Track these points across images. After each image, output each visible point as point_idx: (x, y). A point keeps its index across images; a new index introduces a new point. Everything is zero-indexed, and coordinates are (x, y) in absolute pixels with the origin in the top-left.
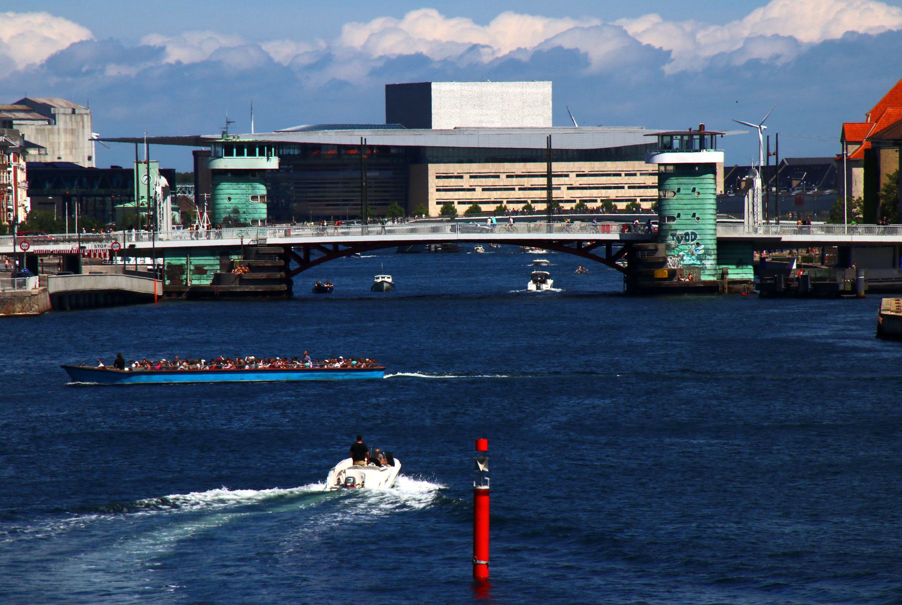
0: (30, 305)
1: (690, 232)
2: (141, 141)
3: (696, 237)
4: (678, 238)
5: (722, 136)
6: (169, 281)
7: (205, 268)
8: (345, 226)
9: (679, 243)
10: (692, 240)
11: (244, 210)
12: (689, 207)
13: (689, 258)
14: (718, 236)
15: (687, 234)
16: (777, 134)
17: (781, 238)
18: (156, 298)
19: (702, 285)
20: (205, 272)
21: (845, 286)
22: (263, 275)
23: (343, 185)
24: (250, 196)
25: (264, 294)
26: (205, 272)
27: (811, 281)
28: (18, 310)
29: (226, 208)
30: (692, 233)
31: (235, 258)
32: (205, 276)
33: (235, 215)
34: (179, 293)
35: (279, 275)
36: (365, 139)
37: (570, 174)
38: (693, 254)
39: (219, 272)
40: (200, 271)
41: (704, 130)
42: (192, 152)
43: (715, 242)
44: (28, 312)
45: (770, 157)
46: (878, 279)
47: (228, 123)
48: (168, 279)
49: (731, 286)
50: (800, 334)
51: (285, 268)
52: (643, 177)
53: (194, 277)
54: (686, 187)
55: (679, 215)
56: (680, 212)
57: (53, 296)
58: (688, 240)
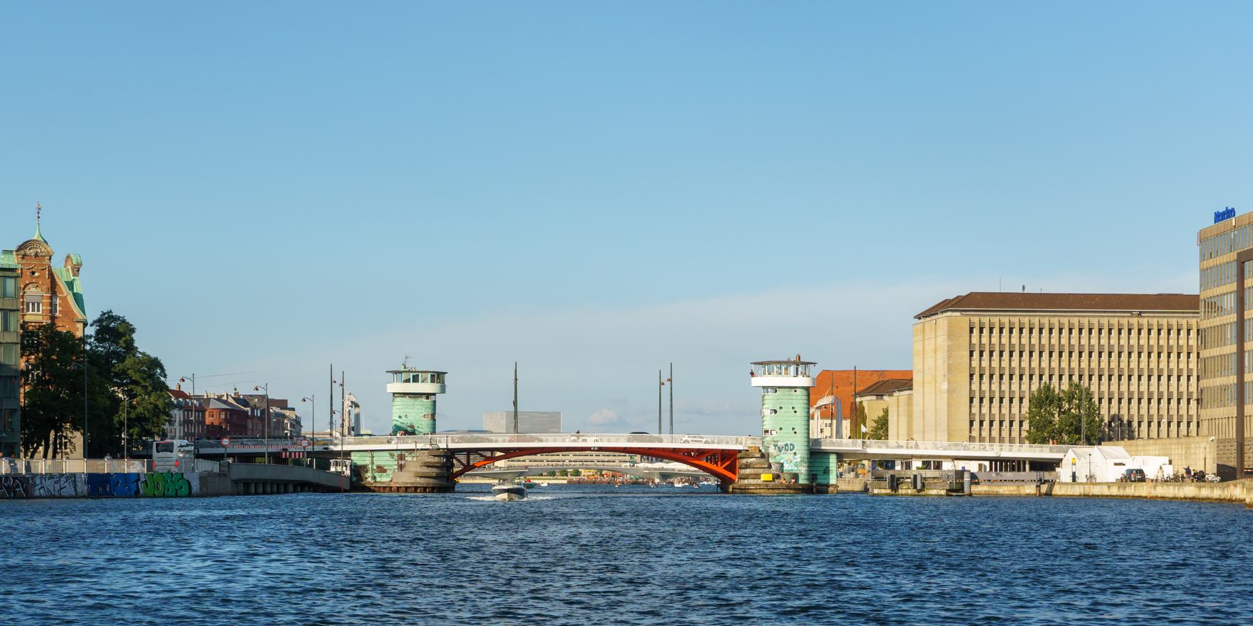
1: (789, 443)
2: (1241, 372)
3: (793, 448)
4: (779, 448)
7: (385, 468)
8: (558, 491)
9: (780, 452)
10: (791, 450)
13: (788, 465)
15: (786, 445)
20: (385, 471)
23: (1188, 562)
26: (385, 471)
30: (791, 444)
36: (1215, 303)
38: (791, 461)
40: (381, 469)
42: (1195, 239)
47: (406, 358)
50: (649, 465)
56: (347, 403)
57: (236, 482)
58: (788, 450)
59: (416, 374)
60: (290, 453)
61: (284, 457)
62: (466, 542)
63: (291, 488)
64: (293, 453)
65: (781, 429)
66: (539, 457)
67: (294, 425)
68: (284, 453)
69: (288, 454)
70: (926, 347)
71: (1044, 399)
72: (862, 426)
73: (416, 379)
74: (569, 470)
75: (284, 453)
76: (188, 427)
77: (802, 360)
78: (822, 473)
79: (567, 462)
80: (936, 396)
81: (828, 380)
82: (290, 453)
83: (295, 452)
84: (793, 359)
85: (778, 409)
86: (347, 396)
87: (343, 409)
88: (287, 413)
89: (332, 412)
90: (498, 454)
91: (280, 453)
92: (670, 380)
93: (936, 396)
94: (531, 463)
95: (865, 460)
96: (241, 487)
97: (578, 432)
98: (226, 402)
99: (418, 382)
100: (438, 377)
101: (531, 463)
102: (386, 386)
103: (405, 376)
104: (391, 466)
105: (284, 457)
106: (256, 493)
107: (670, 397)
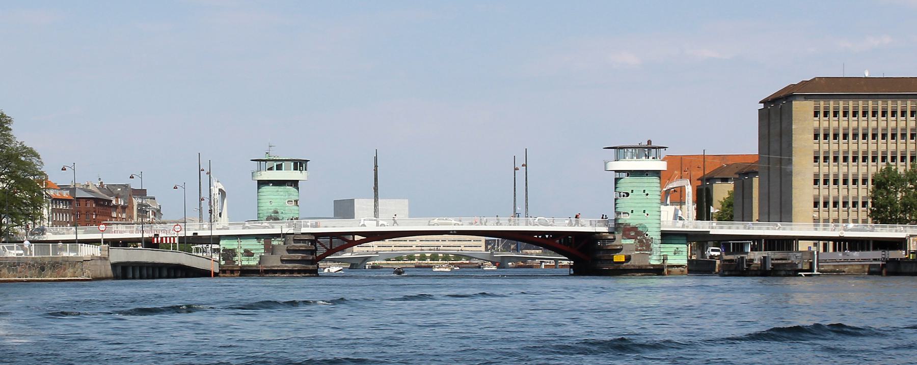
0: (82, 269)
5: (665, 150)
6: (224, 262)
7: (252, 252)
11: (282, 211)
12: (640, 205)
14: (662, 229)
16: (704, 150)
17: (709, 232)
18: (212, 274)
19: (652, 268)
20: (252, 255)
21: (802, 265)
22: (299, 256)
24: (287, 200)
25: (299, 271)
26: (252, 255)
27: (746, 262)
28: (69, 274)
29: (268, 209)
31: (275, 242)
32: (252, 257)
33: (275, 215)
34: (232, 272)
35: (311, 257)
37: (417, 240)
39: (263, 254)
40: (248, 253)
41: (651, 144)
43: (660, 233)
44: (80, 277)
45: (655, 180)
46: (870, 259)
48: (223, 260)
49: (670, 269)
51: (313, 252)
52: (449, 242)
53: (243, 258)
54: (638, 189)
55: (632, 212)
57: (114, 266)
59: (279, 163)
60: (162, 238)
61: (156, 242)
62: (85, 306)
63: (165, 273)
64: (164, 239)
65: (395, 215)
66: (387, 242)
67: (155, 213)
68: (156, 239)
69: (159, 239)
70: (772, 131)
71: (881, 183)
72: (711, 207)
73: (279, 168)
74: (416, 255)
75: (156, 239)
76: (56, 215)
77: (653, 144)
78: (673, 254)
79: (414, 248)
80: (781, 179)
81: (679, 164)
82: (162, 238)
83: (166, 238)
84: (645, 143)
85: (630, 192)
86: (214, 183)
87: (210, 196)
88: (148, 202)
89: (201, 199)
90: (357, 238)
91: (151, 239)
92: (516, 169)
93: (781, 179)
94: (379, 249)
95: (710, 241)
96: (119, 270)
97: (497, 216)
98: (90, 192)
99: (282, 170)
100: (299, 164)
101: (379, 249)
102: (667, 168)
103: (269, 164)
104: (257, 249)
105: (156, 242)
106: (134, 278)
107: (202, 186)
